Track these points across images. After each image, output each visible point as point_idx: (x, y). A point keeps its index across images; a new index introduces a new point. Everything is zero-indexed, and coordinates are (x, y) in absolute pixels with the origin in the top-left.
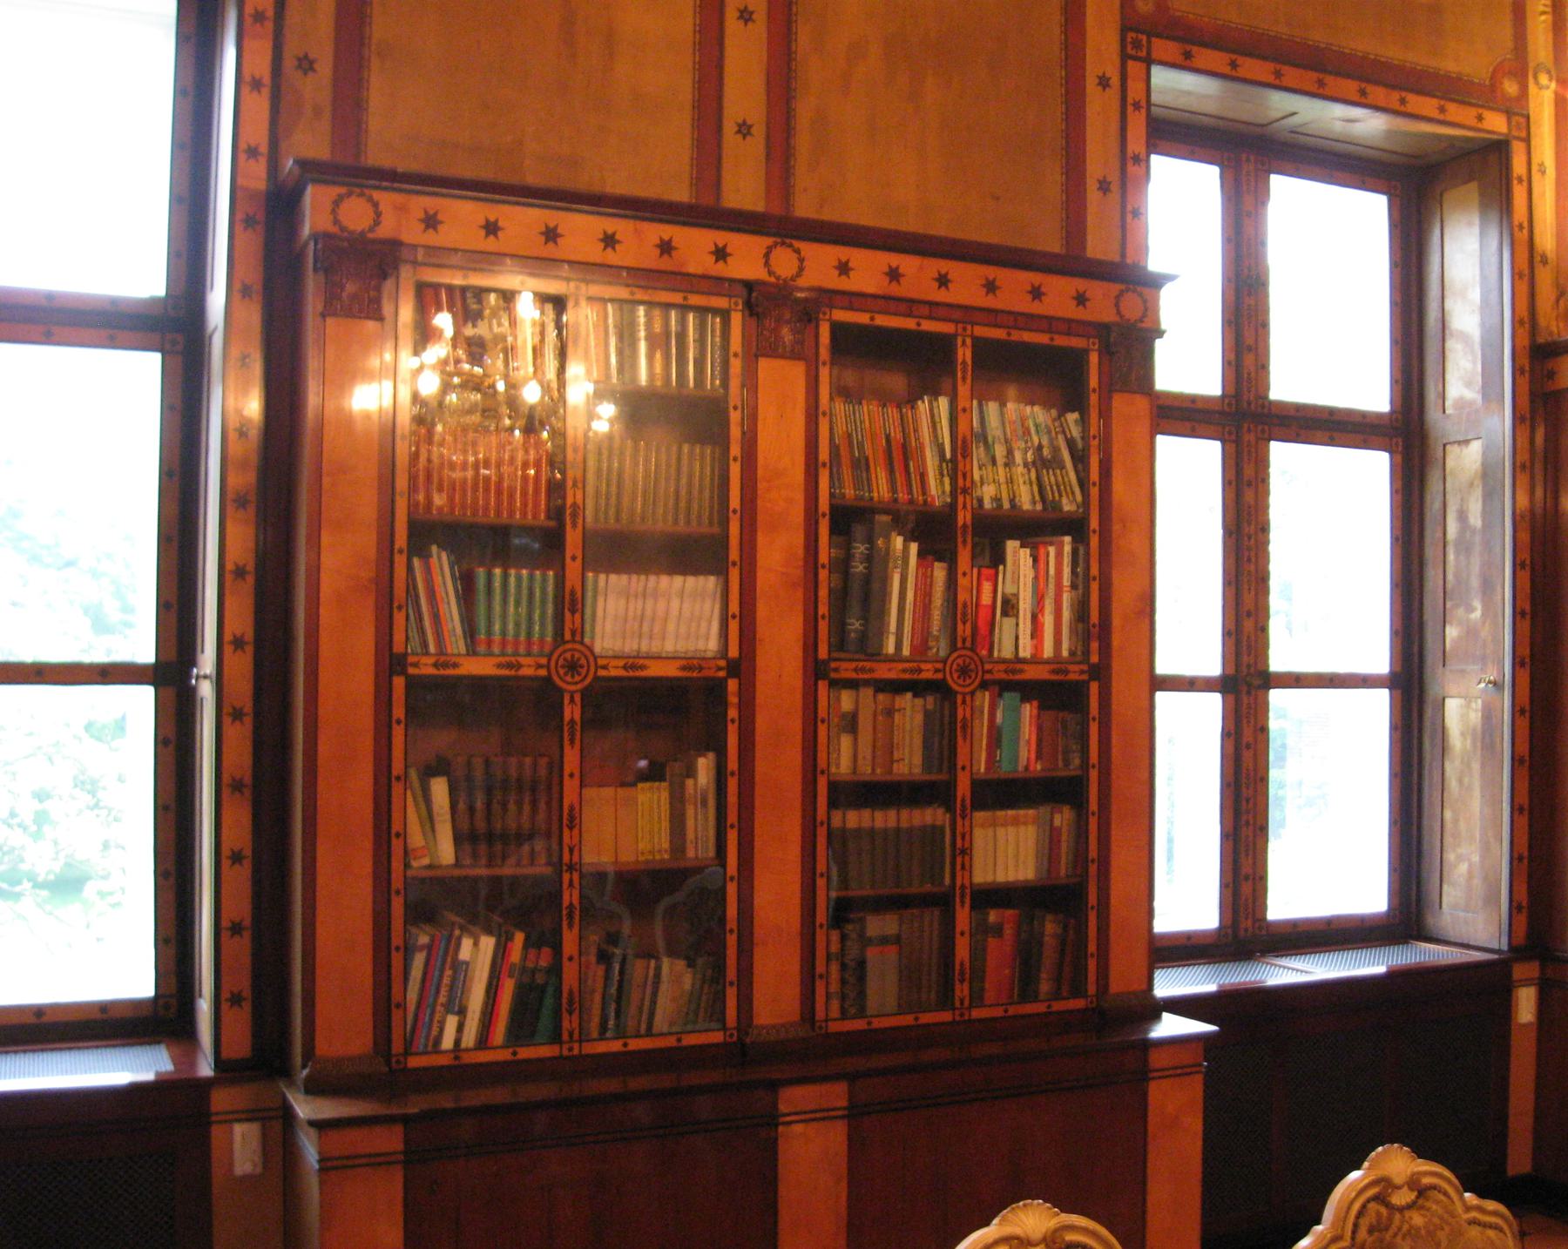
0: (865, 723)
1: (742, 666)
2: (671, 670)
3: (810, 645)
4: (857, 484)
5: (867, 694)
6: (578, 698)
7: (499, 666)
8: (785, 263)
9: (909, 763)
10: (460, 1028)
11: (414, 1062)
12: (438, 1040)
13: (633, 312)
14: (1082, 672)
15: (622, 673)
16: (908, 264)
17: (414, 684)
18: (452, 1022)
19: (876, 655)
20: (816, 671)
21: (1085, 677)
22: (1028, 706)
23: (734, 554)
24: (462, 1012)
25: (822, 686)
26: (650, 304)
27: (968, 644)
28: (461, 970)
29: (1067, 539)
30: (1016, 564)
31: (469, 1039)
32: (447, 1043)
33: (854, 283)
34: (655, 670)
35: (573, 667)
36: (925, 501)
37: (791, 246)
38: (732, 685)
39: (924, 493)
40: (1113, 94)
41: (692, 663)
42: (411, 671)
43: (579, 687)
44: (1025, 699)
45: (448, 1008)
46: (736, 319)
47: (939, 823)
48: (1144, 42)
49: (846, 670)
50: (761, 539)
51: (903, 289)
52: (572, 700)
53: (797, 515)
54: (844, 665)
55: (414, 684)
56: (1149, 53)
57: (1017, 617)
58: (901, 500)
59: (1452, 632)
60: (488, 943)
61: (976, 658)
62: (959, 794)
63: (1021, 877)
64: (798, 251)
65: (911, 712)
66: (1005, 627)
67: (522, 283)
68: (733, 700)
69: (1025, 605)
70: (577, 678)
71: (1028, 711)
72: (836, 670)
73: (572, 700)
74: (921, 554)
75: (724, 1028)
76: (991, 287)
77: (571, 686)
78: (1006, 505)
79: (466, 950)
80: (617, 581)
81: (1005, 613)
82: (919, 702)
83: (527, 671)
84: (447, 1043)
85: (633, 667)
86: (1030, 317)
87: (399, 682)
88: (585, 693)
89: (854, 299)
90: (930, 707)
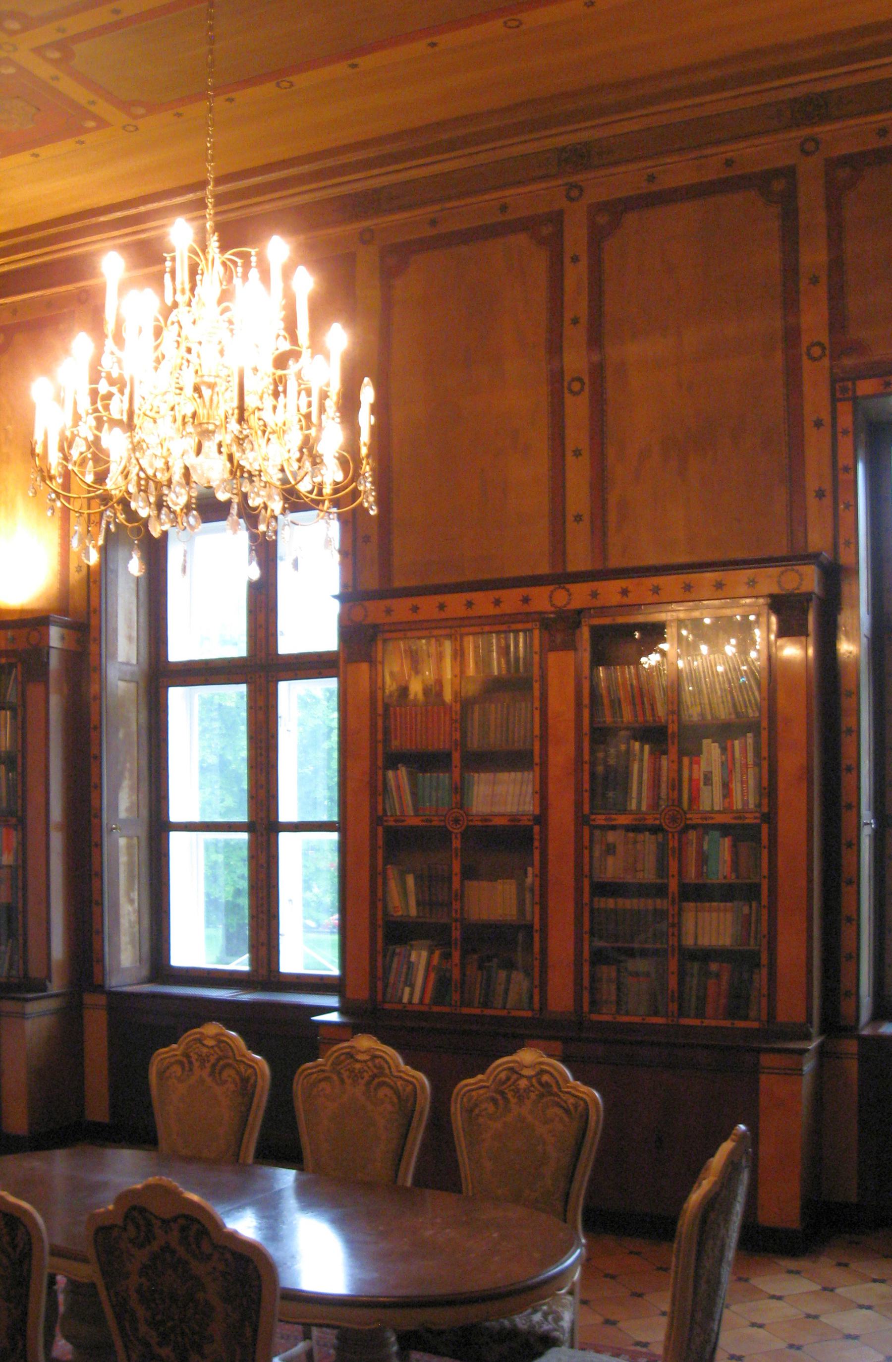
0: (620, 849)
1: (541, 819)
2: (503, 822)
3: (579, 804)
4: (614, 715)
5: (620, 833)
6: (459, 836)
7: (423, 821)
8: (561, 598)
9: (648, 874)
10: (412, 994)
11: (387, 1006)
12: (401, 998)
13: (507, 639)
14: (755, 818)
15: (480, 824)
16: (476, 596)
17: (388, 830)
18: (407, 990)
19: (624, 811)
20: (582, 820)
21: (758, 821)
22: (726, 839)
23: (537, 759)
24: (412, 986)
25: (586, 830)
26: (498, 632)
27: (676, 803)
28: (410, 966)
29: (750, 735)
30: (709, 752)
31: (416, 1000)
32: (405, 999)
33: (396, 617)
34: (496, 822)
35: (456, 821)
36: (654, 720)
37: (564, 588)
38: (537, 828)
39: (653, 715)
40: (826, 431)
41: (514, 818)
42: (385, 824)
43: (460, 830)
44: (724, 835)
45: (406, 984)
46: (536, 633)
47: (665, 908)
48: (847, 395)
49: (600, 820)
50: (551, 750)
51: (448, 614)
52: (456, 837)
53: (571, 735)
54: (599, 817)
55: (388, 830)
56: (840, 400)
57: (712, 785)
58: (608, 722)
59: (121, 735)
60: (424, 954)
61: (681, 811)
62: (670, 890)
63: (721, 943)
64: (568, 590)
65: (648, 843)
66: (705, 792)
67: (702, 614)
68: (537, 837)
69: (717, 779)
70: (458, 826)
71: (727, 842)
72: (594, 820)
73: (456, 837)
74: (652, 753)
75: (533, 1010)
76: (497, 602)
77: (457, 830)
78: (709, 717)
79: (414, 957)
80: (484, 777)
81: (705, 784)
82: (653, 837)
83: (435, 823)
84: (405, 999)
85: (486, 820)
86: (415, 622)
87: (380, 830)
88: (463, 834)
89: (603, 610)
90: (660, 840)
